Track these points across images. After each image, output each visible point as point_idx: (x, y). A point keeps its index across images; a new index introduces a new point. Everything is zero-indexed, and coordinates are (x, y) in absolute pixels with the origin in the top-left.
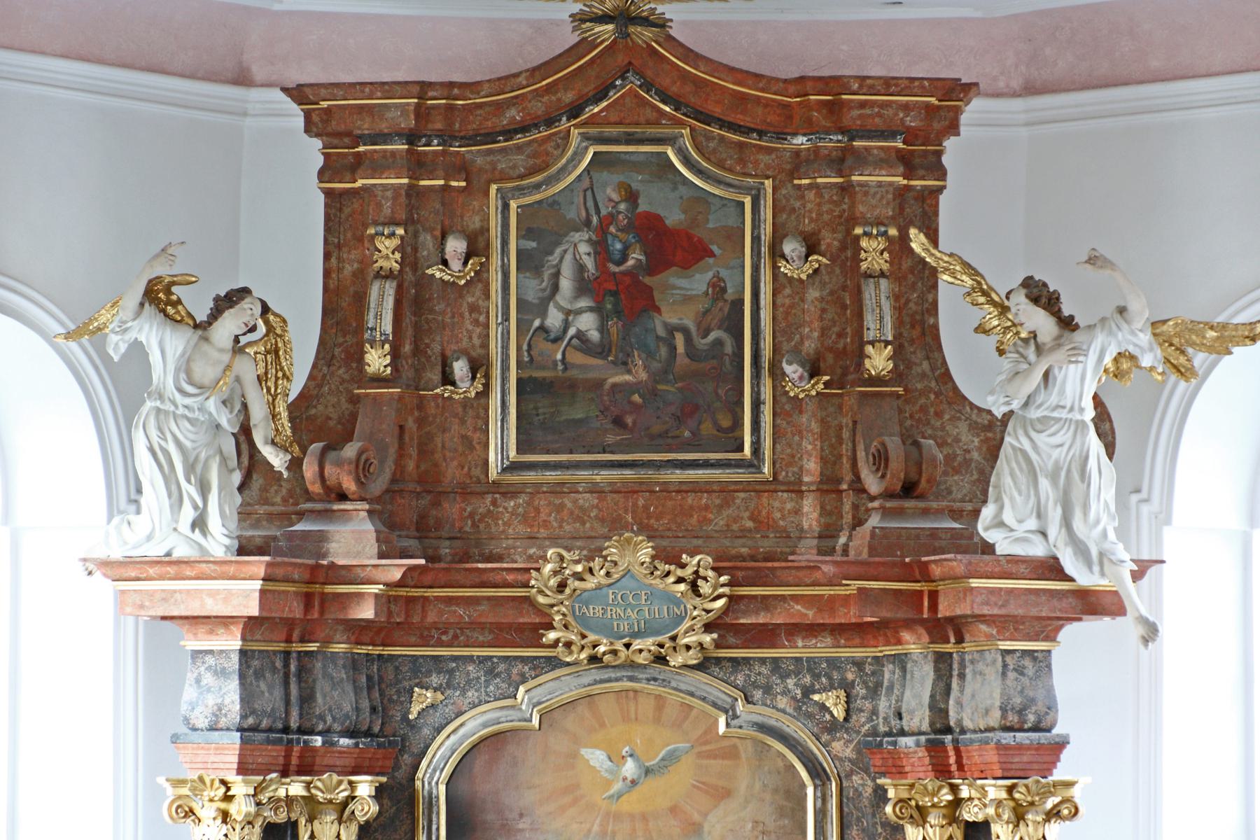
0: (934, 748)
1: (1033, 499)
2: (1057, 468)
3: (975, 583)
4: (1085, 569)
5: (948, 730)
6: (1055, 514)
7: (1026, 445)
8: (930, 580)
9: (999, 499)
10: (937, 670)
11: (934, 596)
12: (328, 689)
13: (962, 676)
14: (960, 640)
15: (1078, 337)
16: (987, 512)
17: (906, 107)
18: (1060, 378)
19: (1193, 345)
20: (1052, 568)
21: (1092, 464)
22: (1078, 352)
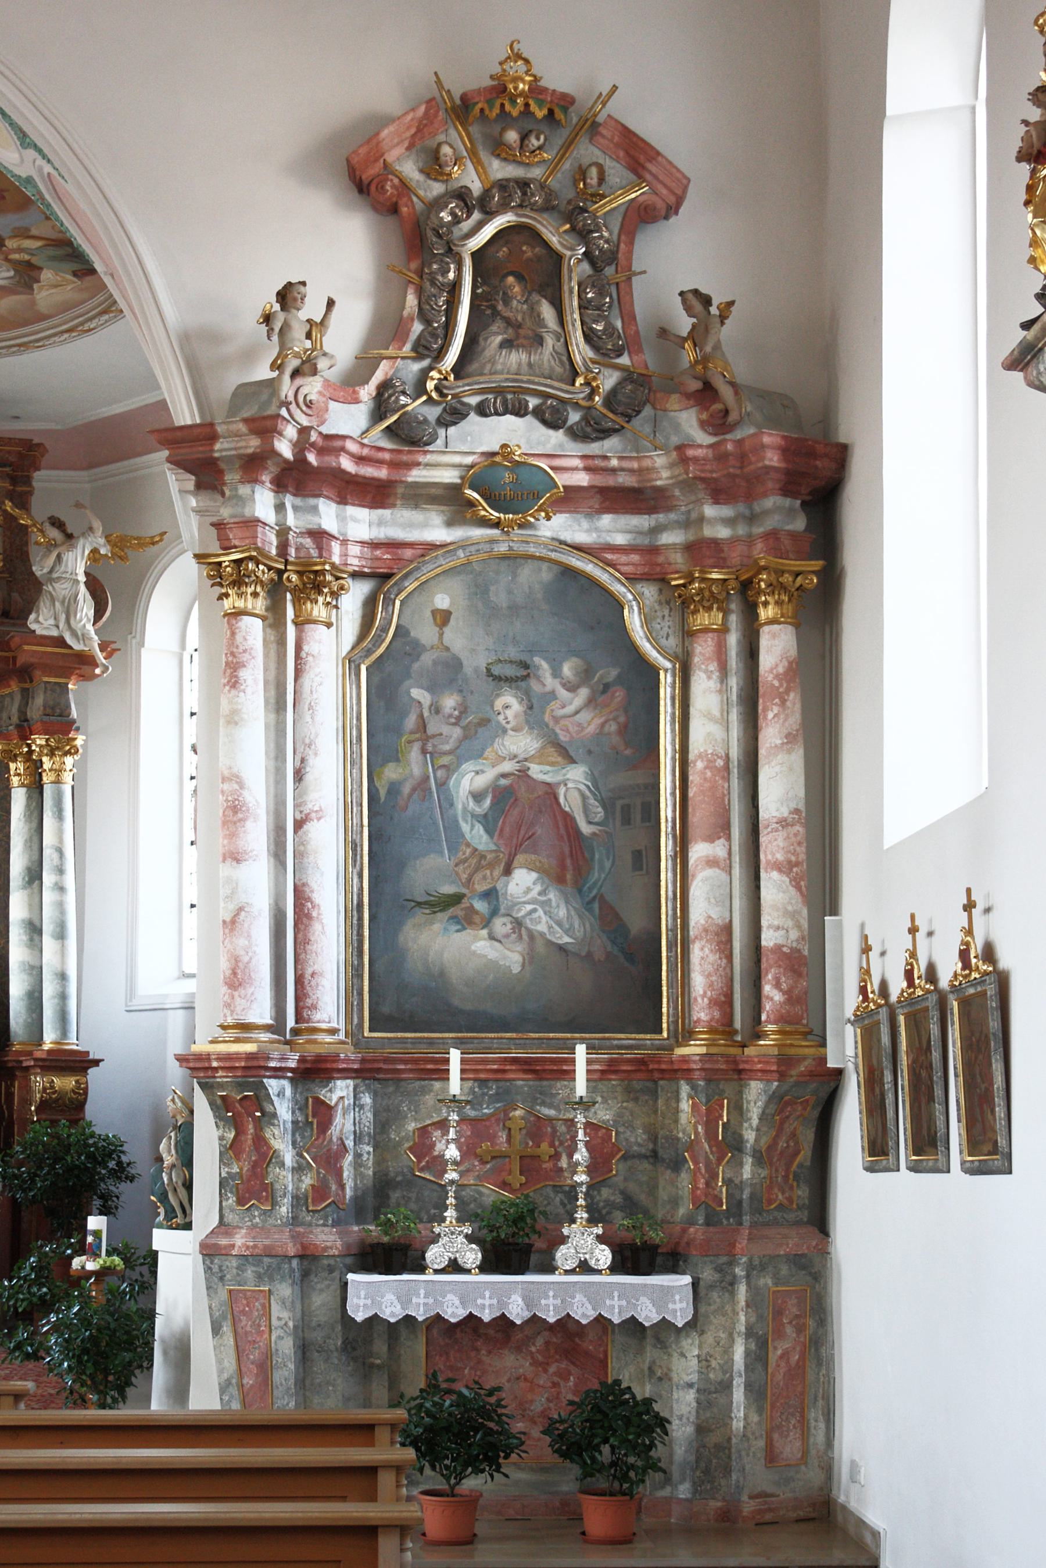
0: (19, 727)
1: (52, 612)
2: (64, 598)
3: (26, 647)
4: (76, 642)
5: (27, 720)
6: (63, 617)
7: (50, 588)
8: (10, 650)
9: (38, 612)
10: (22, 695)
11: (14, 658)
12: (456, 1311)
13: (33, 698)
14: (31, 681)
15: (73, 541)
16: (32, 617)
17: (9, 452)
18: (65, 559)
19: (128, 547)
20: (60, 642)
21: (80, 597)
22: (73, 547)
